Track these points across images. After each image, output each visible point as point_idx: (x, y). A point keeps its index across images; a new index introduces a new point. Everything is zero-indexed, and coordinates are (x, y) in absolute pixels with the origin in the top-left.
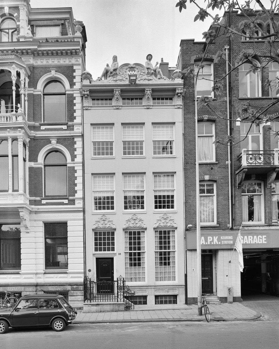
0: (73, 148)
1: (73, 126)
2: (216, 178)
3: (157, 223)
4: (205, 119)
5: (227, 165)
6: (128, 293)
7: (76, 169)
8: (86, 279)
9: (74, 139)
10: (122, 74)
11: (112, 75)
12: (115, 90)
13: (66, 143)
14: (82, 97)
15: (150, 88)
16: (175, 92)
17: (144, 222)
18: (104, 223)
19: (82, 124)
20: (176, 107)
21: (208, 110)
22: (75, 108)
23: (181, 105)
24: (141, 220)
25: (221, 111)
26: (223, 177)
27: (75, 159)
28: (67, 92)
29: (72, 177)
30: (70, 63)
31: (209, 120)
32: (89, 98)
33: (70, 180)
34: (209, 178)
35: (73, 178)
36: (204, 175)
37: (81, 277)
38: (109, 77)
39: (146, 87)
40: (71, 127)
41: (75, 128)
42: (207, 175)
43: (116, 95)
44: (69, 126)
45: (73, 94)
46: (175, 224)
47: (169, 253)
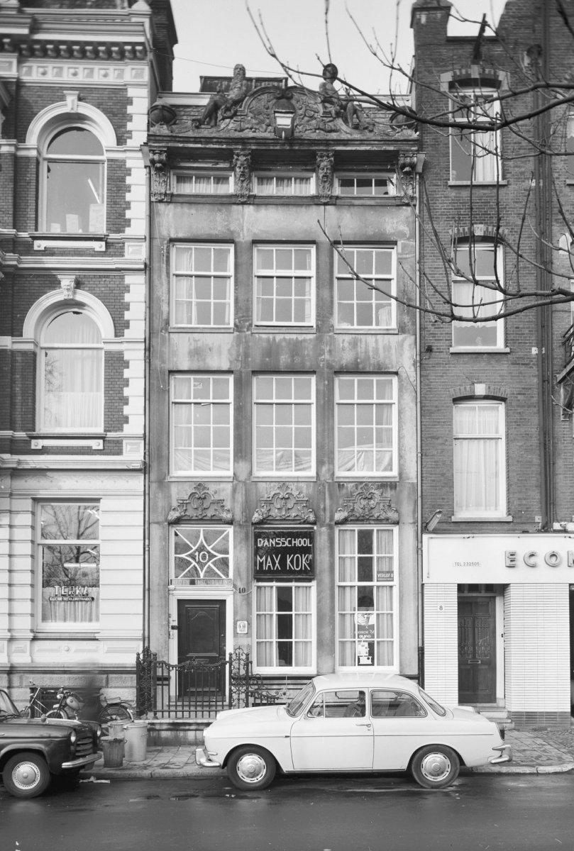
0: (122, 301)
9: (122, 278)
22: (128, 197)
26: (523, 388)
27: (125, 426)
38: (224, 119)
39: (317, 148)
41: (126, 446)
45: (124, 161)
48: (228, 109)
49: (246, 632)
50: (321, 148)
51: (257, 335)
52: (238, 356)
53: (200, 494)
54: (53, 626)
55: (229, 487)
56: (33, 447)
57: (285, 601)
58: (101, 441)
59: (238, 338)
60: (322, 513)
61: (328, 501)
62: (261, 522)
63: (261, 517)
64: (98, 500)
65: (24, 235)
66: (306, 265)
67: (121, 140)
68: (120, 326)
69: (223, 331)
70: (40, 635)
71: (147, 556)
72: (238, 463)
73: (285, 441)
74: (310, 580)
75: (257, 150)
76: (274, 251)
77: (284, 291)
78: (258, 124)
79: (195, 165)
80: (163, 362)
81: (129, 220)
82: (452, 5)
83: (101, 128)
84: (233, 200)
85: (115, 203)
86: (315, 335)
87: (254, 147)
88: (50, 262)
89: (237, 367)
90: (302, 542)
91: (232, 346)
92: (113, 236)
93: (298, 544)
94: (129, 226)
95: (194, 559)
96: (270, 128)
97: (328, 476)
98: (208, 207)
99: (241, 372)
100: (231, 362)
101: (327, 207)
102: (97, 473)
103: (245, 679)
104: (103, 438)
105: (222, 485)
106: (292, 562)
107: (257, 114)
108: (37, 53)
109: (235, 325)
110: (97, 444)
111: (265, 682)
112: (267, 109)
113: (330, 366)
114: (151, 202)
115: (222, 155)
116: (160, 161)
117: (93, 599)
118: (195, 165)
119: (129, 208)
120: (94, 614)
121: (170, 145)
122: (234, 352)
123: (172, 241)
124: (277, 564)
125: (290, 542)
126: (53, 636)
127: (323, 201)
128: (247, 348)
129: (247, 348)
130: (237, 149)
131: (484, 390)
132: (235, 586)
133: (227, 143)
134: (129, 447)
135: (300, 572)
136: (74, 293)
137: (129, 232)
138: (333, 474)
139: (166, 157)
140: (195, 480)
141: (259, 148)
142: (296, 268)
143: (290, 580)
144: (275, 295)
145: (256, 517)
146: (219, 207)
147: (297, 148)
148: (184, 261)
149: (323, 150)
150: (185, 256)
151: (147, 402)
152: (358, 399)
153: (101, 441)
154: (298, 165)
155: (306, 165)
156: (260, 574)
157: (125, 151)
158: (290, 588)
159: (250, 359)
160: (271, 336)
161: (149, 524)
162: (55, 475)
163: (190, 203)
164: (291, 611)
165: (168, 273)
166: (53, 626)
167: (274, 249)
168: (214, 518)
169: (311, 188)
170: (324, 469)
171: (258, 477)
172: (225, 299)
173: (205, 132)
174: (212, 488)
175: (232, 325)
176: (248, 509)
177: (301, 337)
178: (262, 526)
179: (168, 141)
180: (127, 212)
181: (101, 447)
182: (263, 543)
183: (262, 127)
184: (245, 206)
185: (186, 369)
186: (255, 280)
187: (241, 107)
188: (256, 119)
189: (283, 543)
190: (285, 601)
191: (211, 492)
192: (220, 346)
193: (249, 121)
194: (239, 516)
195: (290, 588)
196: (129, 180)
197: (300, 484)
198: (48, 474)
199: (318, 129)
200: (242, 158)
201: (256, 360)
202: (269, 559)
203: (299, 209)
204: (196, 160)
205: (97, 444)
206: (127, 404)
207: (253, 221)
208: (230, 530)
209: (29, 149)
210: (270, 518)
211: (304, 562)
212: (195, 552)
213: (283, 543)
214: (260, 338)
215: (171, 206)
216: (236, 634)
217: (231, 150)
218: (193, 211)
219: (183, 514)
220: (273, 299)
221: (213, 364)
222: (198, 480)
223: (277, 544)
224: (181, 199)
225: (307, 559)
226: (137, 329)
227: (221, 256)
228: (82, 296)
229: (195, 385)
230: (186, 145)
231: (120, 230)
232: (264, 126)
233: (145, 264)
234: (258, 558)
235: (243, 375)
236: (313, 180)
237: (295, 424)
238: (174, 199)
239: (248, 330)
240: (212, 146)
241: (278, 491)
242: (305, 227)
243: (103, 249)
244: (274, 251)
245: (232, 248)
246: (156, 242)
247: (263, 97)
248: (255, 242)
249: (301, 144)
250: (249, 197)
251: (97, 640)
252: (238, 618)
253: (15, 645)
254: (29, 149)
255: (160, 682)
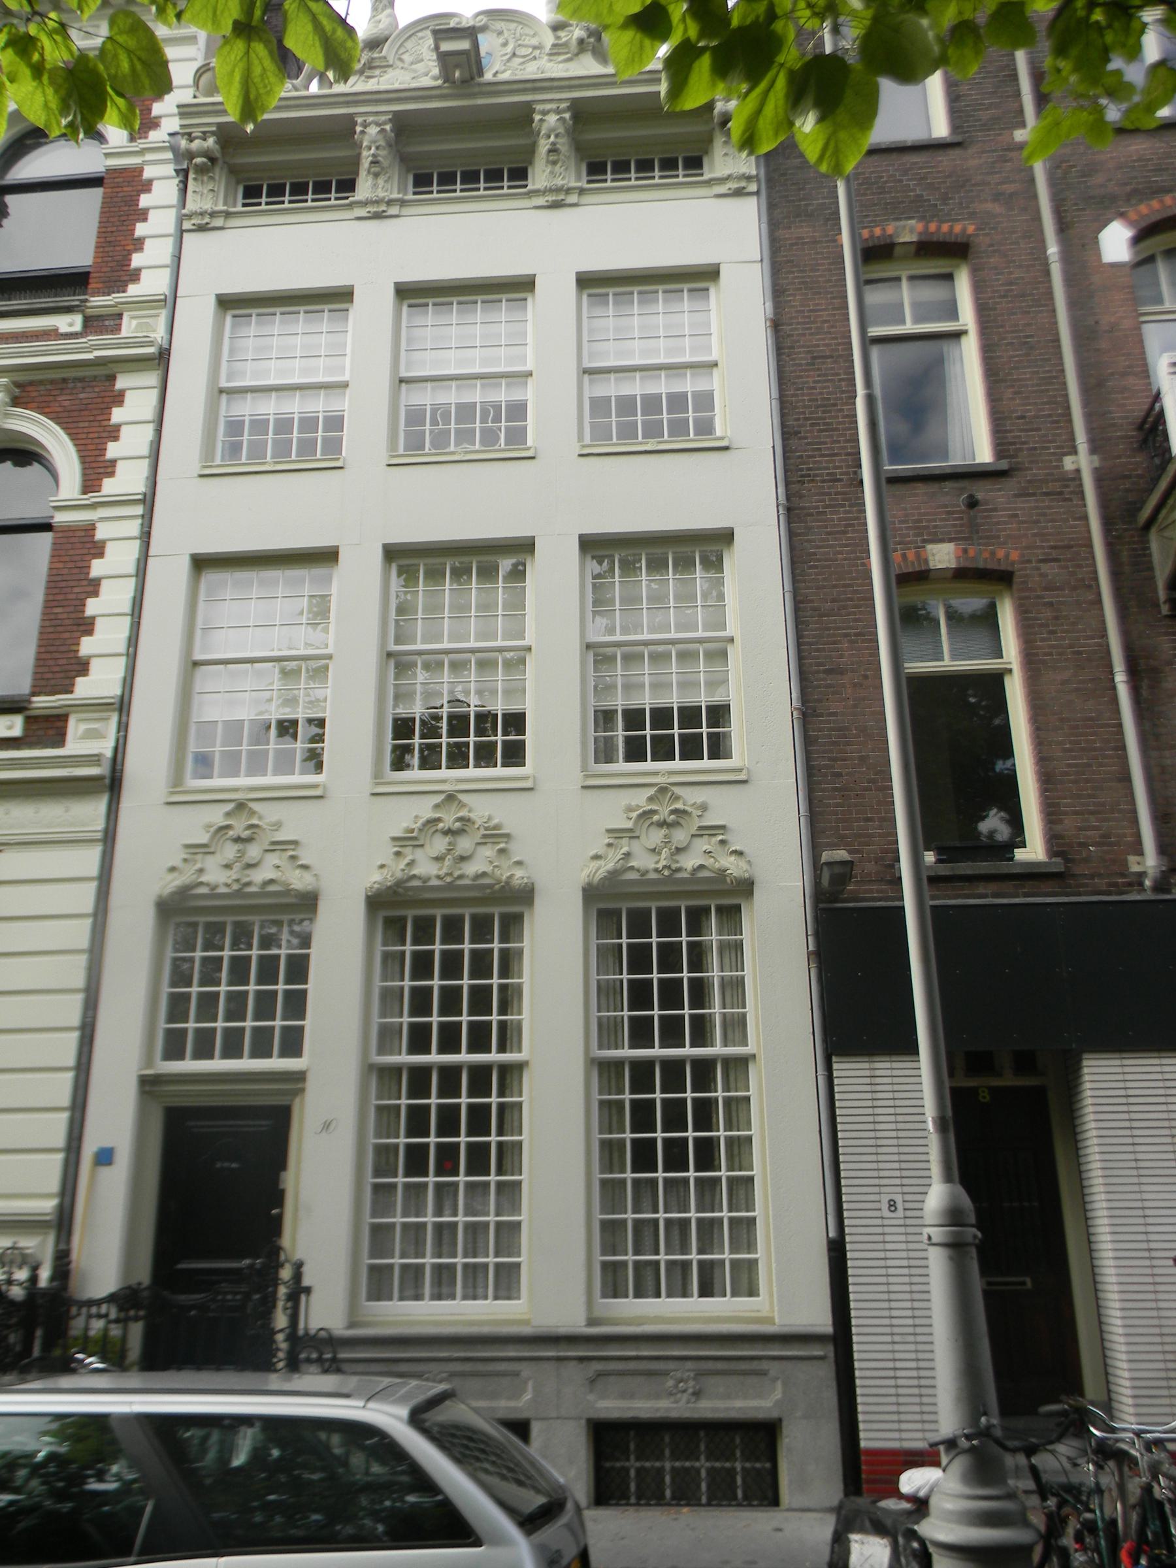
0: (105, 423)
1: (120, 316)
2: (1006, 554)
3: (611, 852)
4: (902, 240)
5: (1073, 479)
7: (100, 535)
9: (112, 378)
10: (412, 63)
12: (360, 120)
13: (67, 403)
14: (183, 174)
15: (560, 100)
16: (712, 118)
17: (513, 846)
18: (242, 854)
19: (170, 302)
20: (722, 189)
21: (917, 196)
23: (749, 178)
24: (495, 836)
25: (997, 197)
26: (1052, 547)
27: (80, 681)
28: (60, 518)
29: (72, 583)
31: (927, 248)
32: (219, 173)
33: (60, 597)
34: (958, 558)
35: (76, 590)
36: (924, 541)
40: (107, 323)
41: (75, 728)
42: (942, 541)
43: (365, 144)
44: (100, 318)
45: (91, 528)
46: (732, 858)
47: (704, 1071)
82: (733, 529)
114: (182, 232)
131: (952, 556)
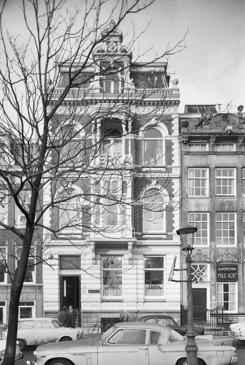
6: (227, 319)
8: (182, 307)
9: (171, 180)
11: (207, 123)
22: (173, 152)
30: (169, 113)
37: (56, 306)
38: (205, 125)
39: (238, 136)
48: (207, 122)
49: (215, 299)
50: (240, 135)
51: (217, 199)
52: (211, 206)
53: (199, 253)
54: (148, 297)
55: (209, 250)
56: (143, 237)
57: (226, 288)
58: (166, 235)
59: (211, 200)
60: (240, 259)
61: (242, 255)
62: (220, 262)
63: (220, 261)
64: (165, 255)
65: (140, 166)
66: (231, 175)
67: (170, 133)
68: (171, 196)
69: (206, 198)
70: (147, 301)
71: (181, 274)
72: (212, 242)
73: (225, 234)
74: (235, 282)
75: (218, 136)
76: (201, 170)
77: (225, 184)
78: (216, 126)
79: (196, 141)
80: (186, 209)
81: (173, 161)
83: (164, 131)
84: (209, 153)
85: (169, 155)
86: (236, 199)
87: (217, 136)
88: (148, 176)
89: (211, 210)
90: (233, 269)
91: (209, 203)
92: (169, 166)
93: (232, 270)
94: (173, 162)
95: (196, 275)
96: (221, 128)
97: (241, 247)
98: (200, 156)
99: (212, 212)
100: (209, 209)
101: (240, 155)
102: (164, 246)
103: (222, 314)
104: (166, 234)
105: (206, 250)
106: (230, 275)
107: (216, 123)
108: (142, 104)
109: (210, 196)
110: (164, 237)
111: (228, 316)
112: (220, 121)
113: (242, 210)
115: (205, 139)
116: (186, 141)
117: (161, 288)
118: (196, 141)
119: (173, 156)
120: (162, 293)
121: (190, 135)
122: (210, 205)
123: (188, 167)
124: (225, 276)
125: (229, 269)
126: (151, 301)
127: (239, 153)
128: (214, 204)
129: (214, 204)
130: (212, 136)
132: (211, 284)
133: (209, 135)
134: (175, 237)
135: (233, 279)
136: (72, 185)
137: (173, 164)
138: (243, 246)
139: (188, 139)
140: (197, 248)
141: (219, 136)
142: (223, 176)
143: (228, 282)
144: (222, 185)
145: (218, 261)
146: (204, 155)
147: (232, 136)
148: (191, 175)
149: (241, 136)
150: (192, 172)
151: (181, 222)
152: (229, 220)
153: (81, 235)
154: (231, 141)
155: (233, 141)
156: (219, 280)
157: (171, 137)
158: (228, 284)
159: (215, 208)
160: (222, 200)
161: (182, 263)
162: (150, 247)
163: (194, 155)
164: (228, 292)
165: (187, 178)
166: (148, 297)
167: (222, 169)
168: (204, 261)
169: (207, 148)
170: (240, 244)
171: (218, 247)
172: (205, 187)
173: (199, 130)
174: (203, 251)
175: (208, 196)
176: (215, 257)
177: (232, 200)
178: (220, 263)
179: (189, 134)
180: (173, 158)
181: (166, 238)
182: (219, 269)
183: (218, 128)
184: (213, 155)
185: (194, 211)
186: (216, 180)
187: (211, 121)
188: (216, 125)
189: (227, 269)
190: (226, 288)
191: (203, 252)
192: (205, 203)
193: (214, 126)
194: (212, 260)
195: (228, 284)
196: (173, 147)
197: (232, 249)
198: (148, 247)
199: (237, 128)
200: (214, 139)
201: (217, 208)
202: (222, 275)
203: (231, 156)
204: (196, 140)
205: (164, 237)
206: (174, 223)
207: (214, 160)
208: (208, 265)
209: (139, 137)
210: (223, 261)
211: (234, 276)
212: (196, 272)
213: (227, 269)
214: (218, 201)
215: (188, 156)
216: (211, 300)
217: (210, 137)
218: (195, 157)
219: (194, 260)
220: (227, 187)
221: (203, 210)
222: (199, 248)
223: (225, 269)
224: (191, 153)
225: (235, 274)
226: (177, 199)
227: (204, 172)
228: (159, 187)
229: (196, 216)
230: (195, 135)
231: (170, 164)
232: (219, 127)
233: (180, 176)
234: (219, 274)
235: (213, 213)
236: (235, 145)
237: (223, 229)
238: (189, 153)
239: (214, 198)
240: (204, 136)
241: (225, 252)
242: (233, 162)
243: (165, 170)
244: (201, 170)
245: (208, 169)
246: (183, 168)
247: (218, 117)
248: (216, 167)
249: (233, 134)
250: (215, 152)
251: (165, 302)
252: (212, 294)
253: (138, 304)
254: (139, 137)
255: (214, 316)
